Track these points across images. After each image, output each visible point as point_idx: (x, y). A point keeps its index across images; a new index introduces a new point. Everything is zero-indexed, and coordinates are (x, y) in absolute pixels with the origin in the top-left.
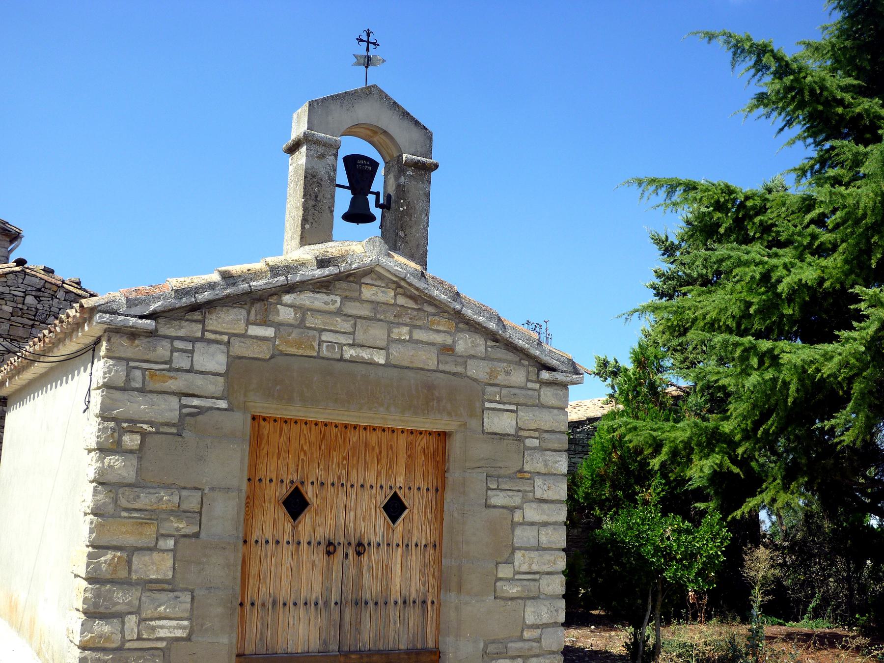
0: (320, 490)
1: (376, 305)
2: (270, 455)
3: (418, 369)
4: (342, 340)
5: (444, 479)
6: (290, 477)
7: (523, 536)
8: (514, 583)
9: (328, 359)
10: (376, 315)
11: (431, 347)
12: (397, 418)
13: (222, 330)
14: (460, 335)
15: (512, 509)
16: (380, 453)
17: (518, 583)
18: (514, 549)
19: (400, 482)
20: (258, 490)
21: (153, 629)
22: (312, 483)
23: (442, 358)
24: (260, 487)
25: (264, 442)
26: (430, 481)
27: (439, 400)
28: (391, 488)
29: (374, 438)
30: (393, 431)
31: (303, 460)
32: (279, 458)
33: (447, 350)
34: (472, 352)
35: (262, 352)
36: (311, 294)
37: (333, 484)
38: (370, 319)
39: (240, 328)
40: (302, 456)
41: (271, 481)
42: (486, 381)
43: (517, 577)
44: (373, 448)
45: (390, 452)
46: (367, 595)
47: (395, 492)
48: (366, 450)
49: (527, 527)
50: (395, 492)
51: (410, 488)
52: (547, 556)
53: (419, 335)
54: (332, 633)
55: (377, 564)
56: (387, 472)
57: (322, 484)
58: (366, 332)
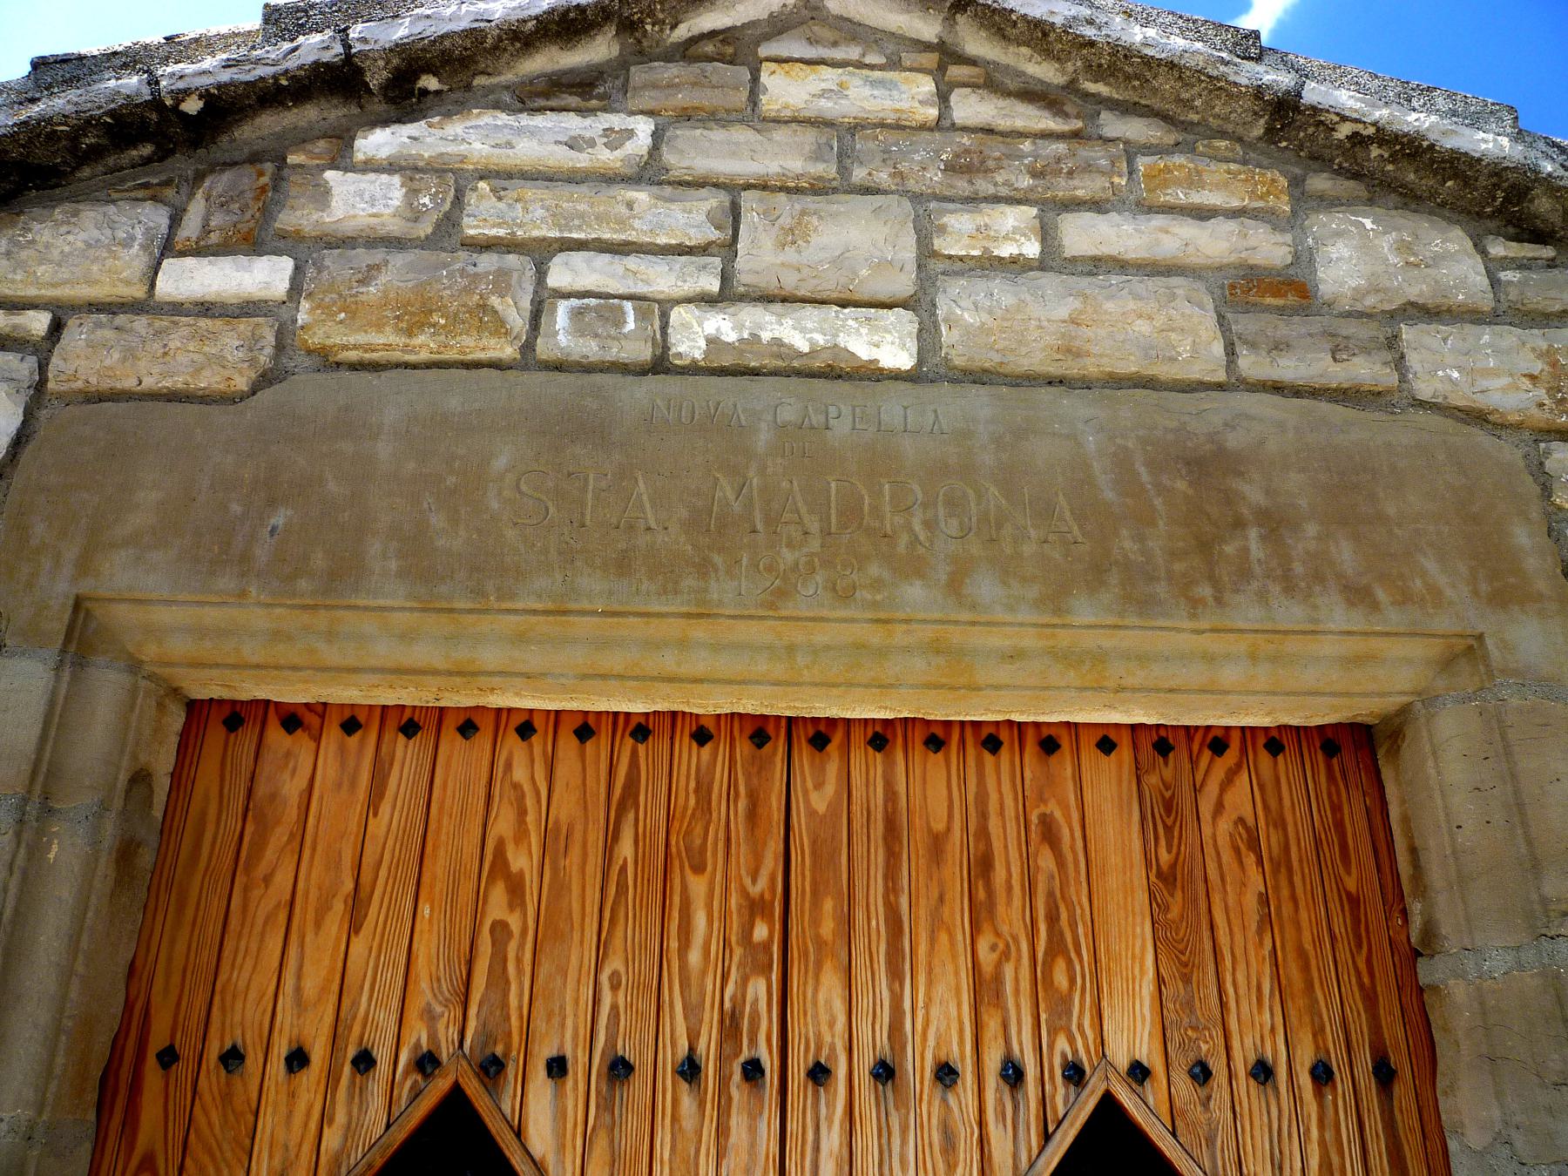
0: (607, 1105)
1: (842, 135)
2: (305, 912)
3: (1117, 382)
4: (662, 278)
5: (1418, 1006)
6: (417, 1034)
9: (587, 368)
10: (844, 171)
11: (1175, 281)
12: (1029, 640)
13: (32, 292)
14: (1322, 223)
16: (983, 866)
19: (1131, 1033)
20: (210, 1117)
22: (557, 1067)
23: (1244, 324)
24: (227, 1097)
25: (279, 836)
26: (1329, 1016)
28: (1075, 1074)
29: (933, 789)
30: (1049, 745)
31: (500, 928)
32: (354, 925)
33: (1253, 293)
34: (1417, 290)
35: (224, 360)
36: (503, 118)
37: (690, 1070)
38: (819, 189)
39: (117, 274)
40: (497, 905)
41: (298, 1059)
42: (1540, 417)
44: (937, 845)
45: (1046, 861)
47: (1108, 1102)
48: (892, 856)
50: (1108, 1102)
51: (1201, 1073)
53: (1083, 234)
56: (1040, 981)
57: (620, 1069)
58: (792, 236)
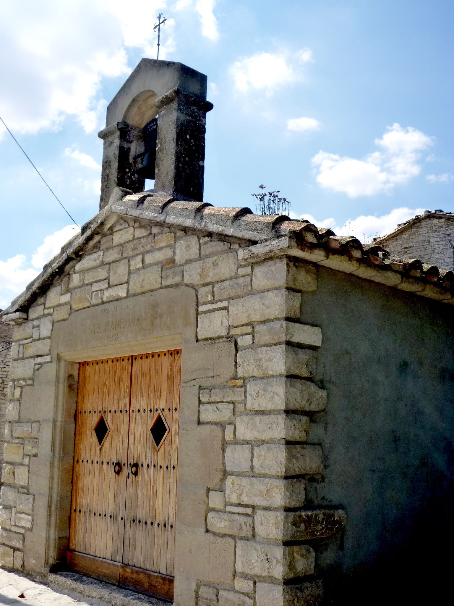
7: (236, 459)
8: (223, 515)
15: (222, 425)
17: (226, 517)
18: (225, 473)
21: (20, 519)
27: (161, 316)
43: (229, 509)
46: (140, 515)
49: (239, 447)
52: (260, 485)
54: (119, 545)
55: (147, 485)
